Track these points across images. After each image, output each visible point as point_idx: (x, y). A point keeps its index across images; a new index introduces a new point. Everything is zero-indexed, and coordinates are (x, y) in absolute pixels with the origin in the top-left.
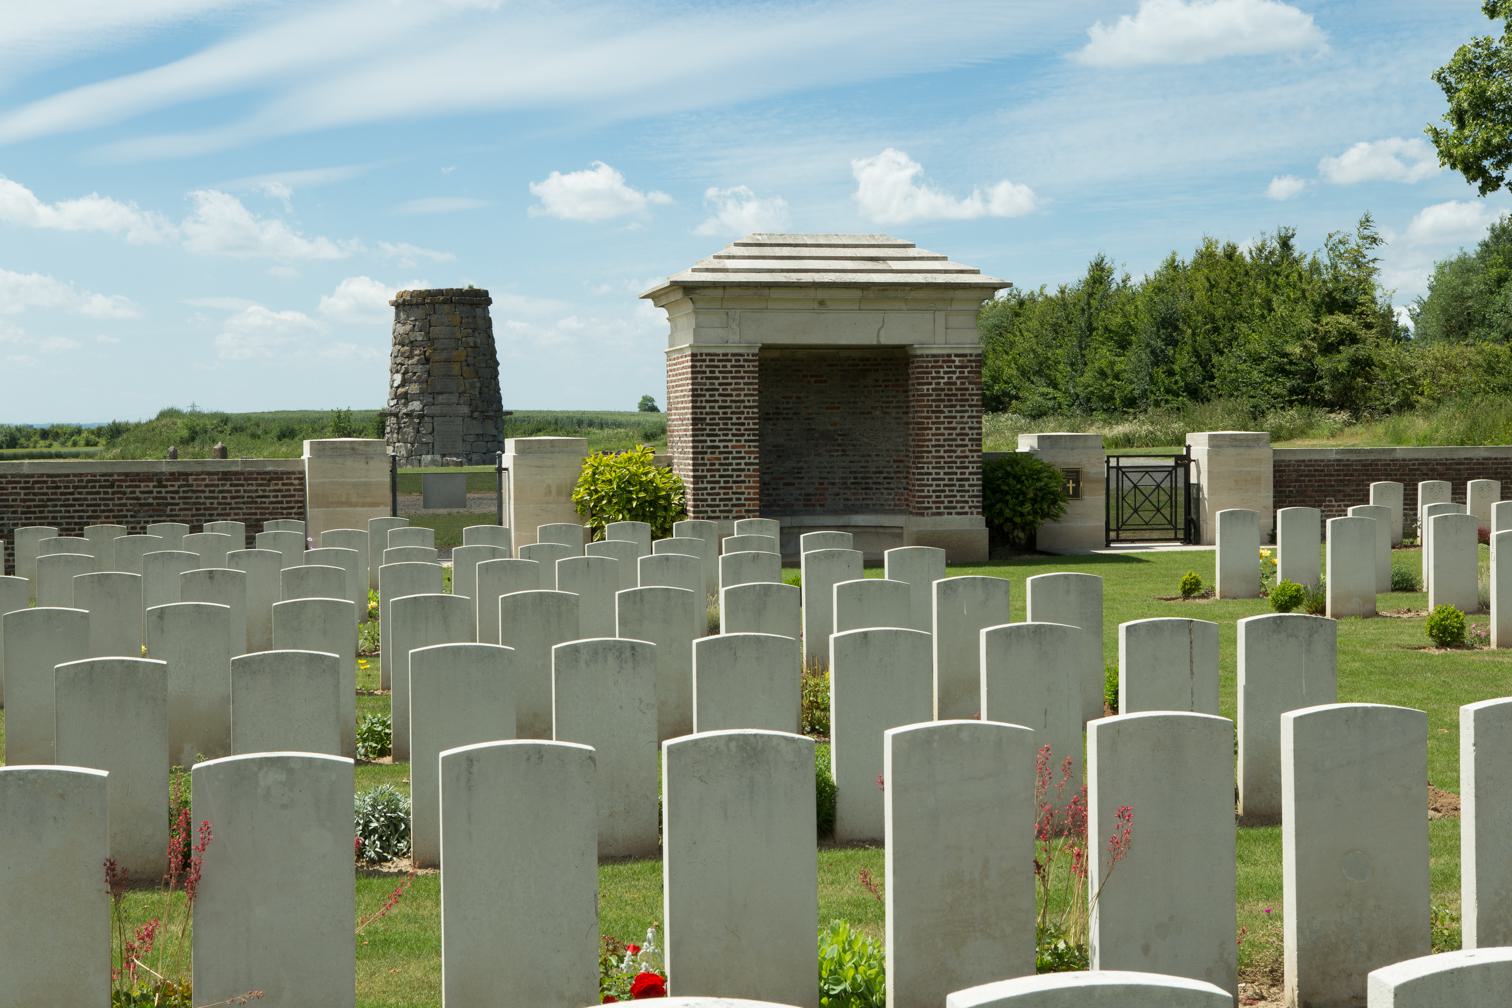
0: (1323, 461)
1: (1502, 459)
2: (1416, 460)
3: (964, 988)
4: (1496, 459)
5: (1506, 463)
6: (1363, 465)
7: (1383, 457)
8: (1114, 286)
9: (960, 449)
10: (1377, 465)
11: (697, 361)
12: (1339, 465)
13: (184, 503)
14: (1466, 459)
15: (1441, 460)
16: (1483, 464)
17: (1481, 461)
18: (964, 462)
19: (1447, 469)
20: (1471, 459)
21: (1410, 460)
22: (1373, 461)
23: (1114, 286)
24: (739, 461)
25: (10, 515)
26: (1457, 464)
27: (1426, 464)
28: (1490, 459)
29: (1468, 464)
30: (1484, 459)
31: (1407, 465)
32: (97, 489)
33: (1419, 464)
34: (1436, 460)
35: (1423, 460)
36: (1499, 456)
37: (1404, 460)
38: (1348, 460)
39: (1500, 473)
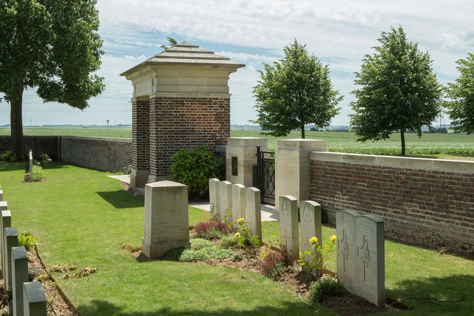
0: (336, 163)
1: (448, 173)
2: (387, 168)
3: (21, 122)
4: (443, 173)
5: (451, 178)
6: (357, 169)
7: (456, 171)
8: (433, 283)
9: (139, 129)
10: (364, 169)
11: (139, 159)
12: (344, 167)
13: (170, 106)
14: (420, 170)
15: (403, 170)
16: (433, 177)
17: (432, 174)
18: (143, 145)
19: (408, 179)
20: (424, 171)
21: (383, 168)
22: (362, 166)
23: (433, 283)
24: (210, 108)
25: (184, 111)
26: (416, 175)
27: (394, 172)
28: (438, 172)
29: (422, 175)
30: (434, 172)
31: (381, 172)
32: (207, 140)
33: (389, 172)
34: (400, 169)
35: (391, 168)
36: (446, 170)
37: (380, 167)
38: (349, 164)
39: (447, 187)
